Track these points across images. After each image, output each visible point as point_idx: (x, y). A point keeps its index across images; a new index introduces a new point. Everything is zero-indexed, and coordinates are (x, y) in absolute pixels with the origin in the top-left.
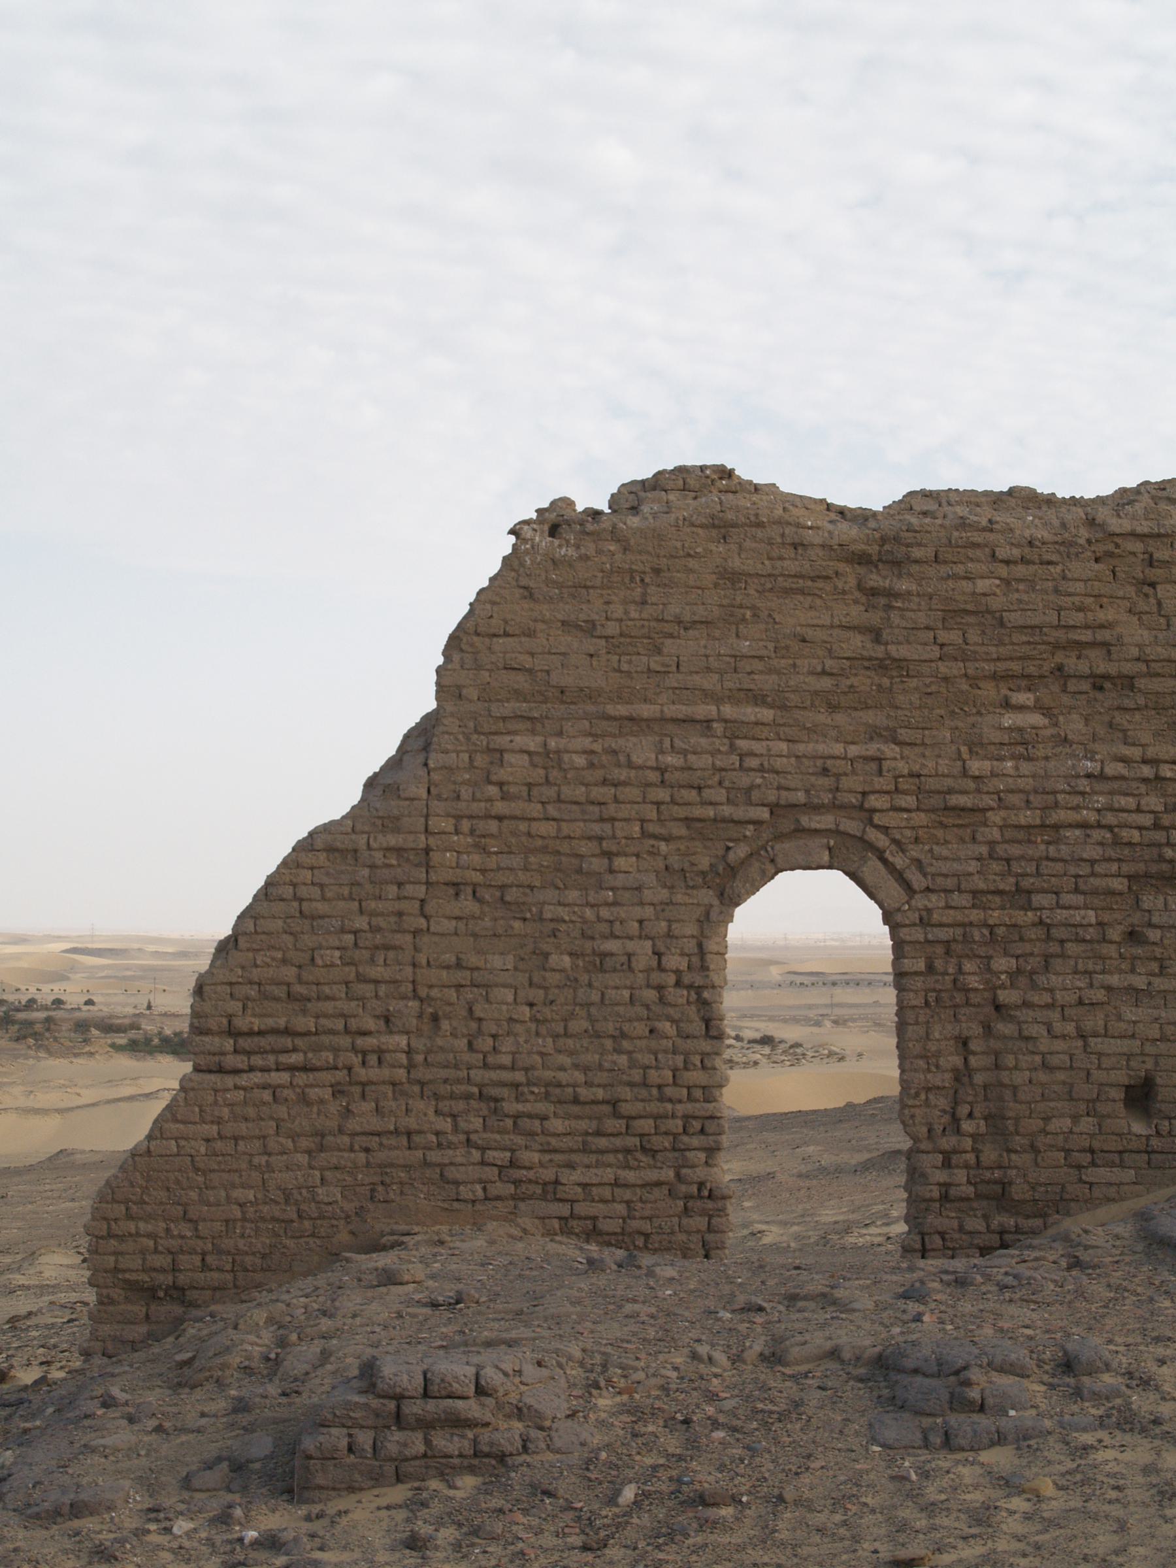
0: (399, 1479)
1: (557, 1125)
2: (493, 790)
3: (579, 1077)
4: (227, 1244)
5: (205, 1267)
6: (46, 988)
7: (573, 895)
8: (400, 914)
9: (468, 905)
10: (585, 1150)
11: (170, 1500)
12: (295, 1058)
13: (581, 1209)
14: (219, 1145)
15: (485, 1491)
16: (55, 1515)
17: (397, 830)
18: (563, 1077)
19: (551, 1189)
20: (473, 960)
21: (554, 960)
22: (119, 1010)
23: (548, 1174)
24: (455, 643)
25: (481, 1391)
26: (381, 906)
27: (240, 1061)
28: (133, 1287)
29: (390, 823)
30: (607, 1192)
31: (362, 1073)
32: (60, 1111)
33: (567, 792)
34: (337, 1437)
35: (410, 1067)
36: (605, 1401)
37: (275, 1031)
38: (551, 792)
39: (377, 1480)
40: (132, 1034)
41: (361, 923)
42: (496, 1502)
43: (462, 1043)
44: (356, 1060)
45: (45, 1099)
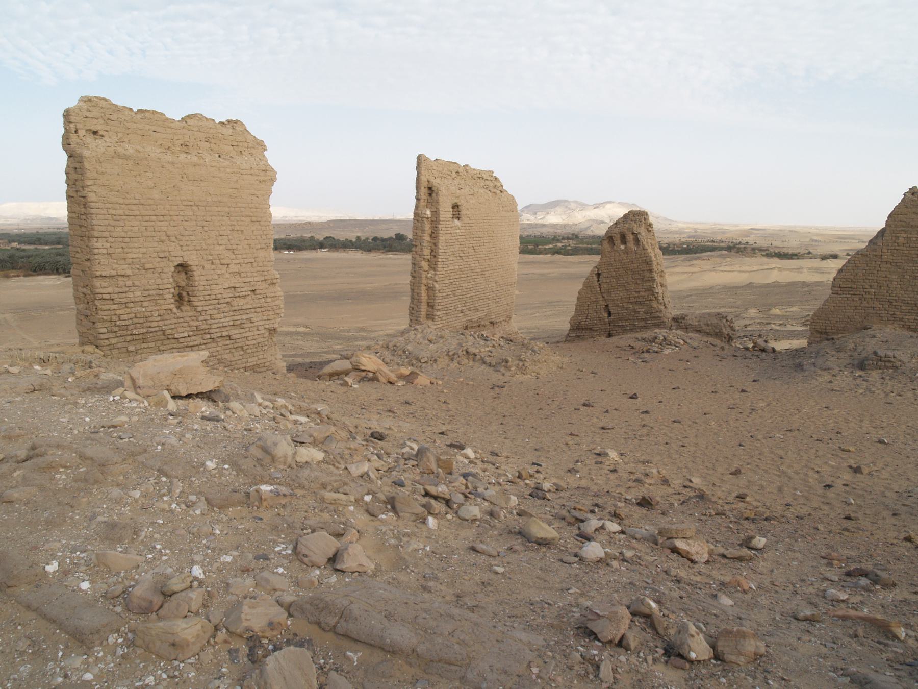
0: (880, 369)
1: (903, 308)
2: (896, 244)
3: (909, 299)
4: (836, 325)
5: (832, 329)
6: (744, 239)
7: (911, 265)
8: (875, 267)
9: (889, 266)
10: (909, 313)
11: (843, 369)
12: (852, 293)
13: (907, 323)
14: (836, 307)
15: (894, 372)
16: (825, 370)
17: (876, 251)
18: (906, 299)
19: (901, 319)
20: (889, 276)
21: (906, 277)
22: (763, 245)
23: (901, 317)
24: (890, 216)
25: (894, 357)
26: (871, 265)
27: (841, 293)
28: (818, 332)
29: (875, 250)
30: (912, 321)
31: (865, 296)
32: (748, 272)
33: (911, 245)
34: (870, 362)
35: (875, 295)
36: (914, 360)
37: (849, 287)
38: (908, 245)
39: (876, 369)
40: (767, 252)
41: (867, 268)
42: (896, 374)
43: (886, 291)
44: (864, 293)
45: (744, 268)
